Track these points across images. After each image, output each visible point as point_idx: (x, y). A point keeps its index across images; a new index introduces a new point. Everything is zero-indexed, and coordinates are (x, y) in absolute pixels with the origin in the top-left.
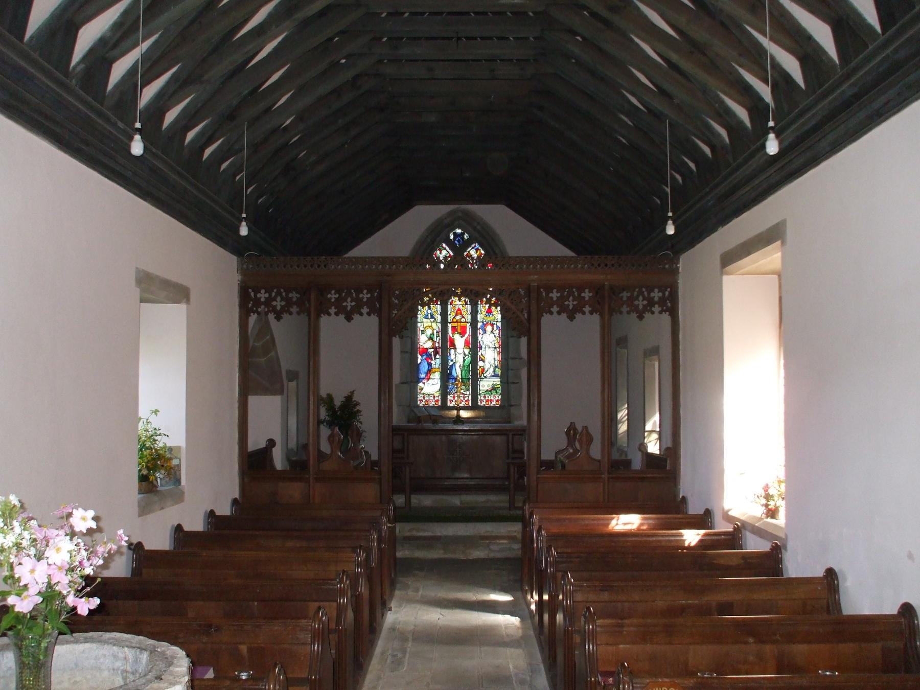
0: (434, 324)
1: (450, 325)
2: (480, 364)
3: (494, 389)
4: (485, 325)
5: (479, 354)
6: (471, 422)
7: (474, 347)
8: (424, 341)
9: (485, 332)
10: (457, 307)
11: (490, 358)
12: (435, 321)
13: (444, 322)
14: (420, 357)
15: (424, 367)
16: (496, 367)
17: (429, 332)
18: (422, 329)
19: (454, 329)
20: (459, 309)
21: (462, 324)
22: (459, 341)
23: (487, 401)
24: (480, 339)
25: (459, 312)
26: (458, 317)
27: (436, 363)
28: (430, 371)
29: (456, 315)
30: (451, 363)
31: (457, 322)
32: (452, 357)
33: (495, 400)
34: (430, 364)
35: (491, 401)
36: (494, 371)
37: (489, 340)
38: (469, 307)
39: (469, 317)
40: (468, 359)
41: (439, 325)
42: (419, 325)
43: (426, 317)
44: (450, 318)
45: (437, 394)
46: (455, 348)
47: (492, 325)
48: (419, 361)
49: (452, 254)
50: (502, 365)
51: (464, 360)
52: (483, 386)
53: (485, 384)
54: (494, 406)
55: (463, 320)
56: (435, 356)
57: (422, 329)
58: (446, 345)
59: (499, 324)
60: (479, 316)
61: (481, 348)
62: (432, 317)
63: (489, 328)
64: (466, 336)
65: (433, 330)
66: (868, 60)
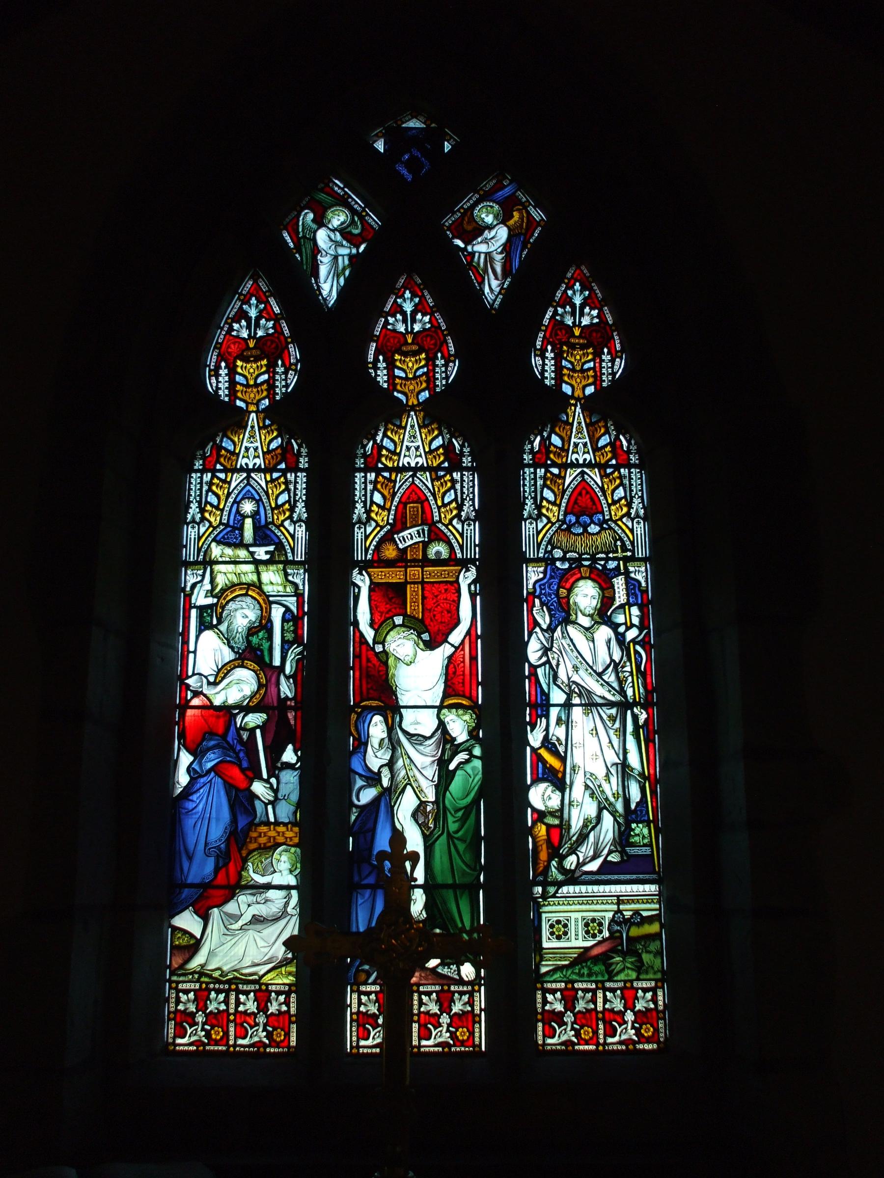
0: (272, 578)
1: (362, 582)
2: (541, 796)
3: (620, 944)
4: (562, 581)
5: (535, 738)
6: (312, 262)
7: (501, 697)
8: (212, 667)
9: (564, 615)
10: (402, 482)
11: (594, 760)
12: (279, 558)
13: (329, 561)
14: (185, 759)
15: (208, 819)
16: (630, 816)
17: (243, 615)
18: (201, 598)
19: (388, 600)
20: (415, 495)
21: (433, 573)
22: (419, 673)
23: (586, 1018)
24: (533, 652)
25: (412, 509)
26: (410, 537)
27: (277, 793)
28: (244, 839)
29: (399, 525)
30: (367, 796)
31: (402, 560)
32: (376, 759)
33: (629, 1016)
34: (241, 801)
35: (612, 1019)
36: (623, 839)
37: (585, 652)
38: (469, 485)
39: (474, 532)
40: (470, 772)
41: (300, 577)
42: (190, 578)
43: (230, 536)
44: (365, 538)
45: (283, 979)
46: (391, 707)
47: (604, 580)
48: (183, 779)
49: (373, 220)
50: (668, 806)
51: (445, 778)
52: (561, 930)
53: (571, 919)
54: (629, 1052)
55: (438, 549)
56: (274, 752)
57: (201, 598)
58: (328, 693)
59: (640, 574)
60: (528, 529)
61: (543, 706)
62: (263, 535)
63: (586, 595)
64: (457, 636)
65: (267, 602)
66: (351, 1032)
